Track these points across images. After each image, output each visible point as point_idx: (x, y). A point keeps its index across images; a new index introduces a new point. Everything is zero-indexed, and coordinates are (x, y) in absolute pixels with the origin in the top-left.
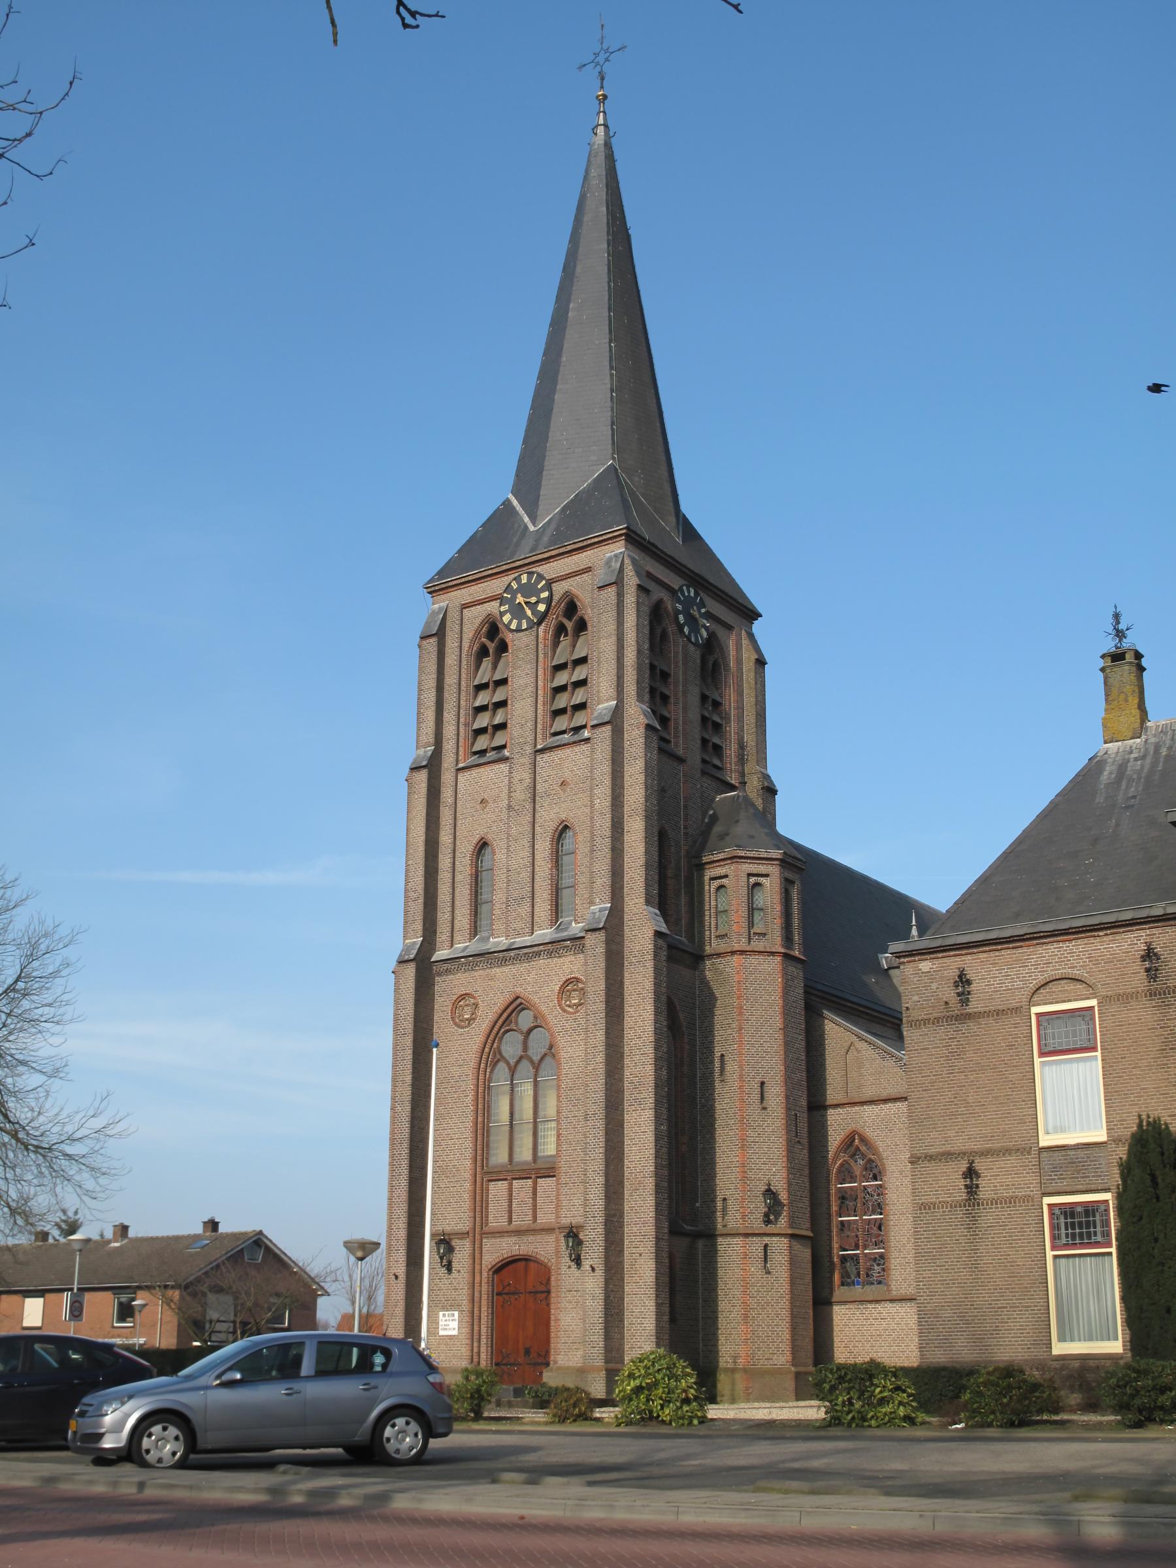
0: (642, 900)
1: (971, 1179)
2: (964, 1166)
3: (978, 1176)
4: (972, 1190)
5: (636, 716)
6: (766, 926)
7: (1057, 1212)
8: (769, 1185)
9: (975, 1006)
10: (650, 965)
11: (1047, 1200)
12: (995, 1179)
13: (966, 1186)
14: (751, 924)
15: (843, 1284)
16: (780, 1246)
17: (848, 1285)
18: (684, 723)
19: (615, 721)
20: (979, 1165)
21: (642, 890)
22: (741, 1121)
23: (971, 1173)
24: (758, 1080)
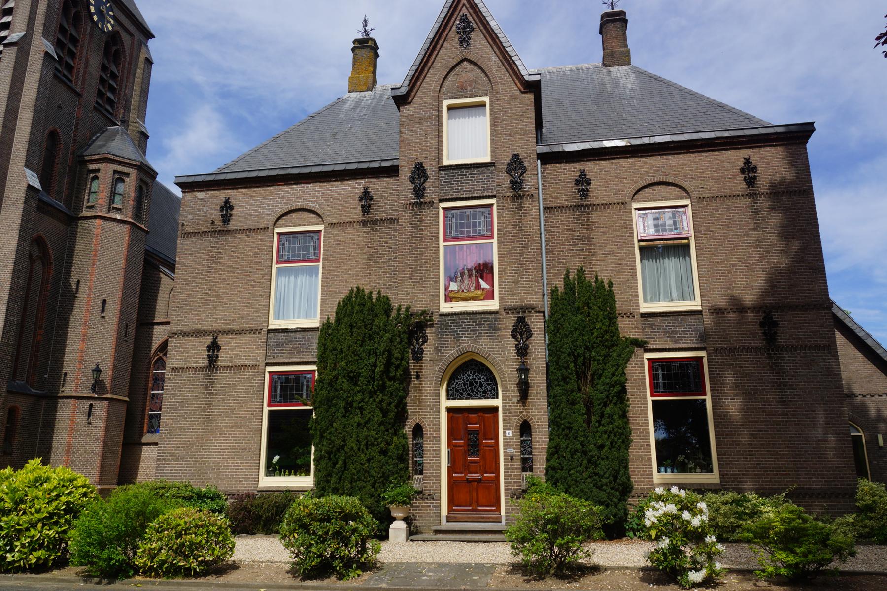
0: (23, 164)
1: (214, 351)
2: (209, 340)
3: (219, 350)
4: (213, 359)
5: (41, 45)
6: (123, 203)
7: (276, 377)
8: (97, 365)
9: (234, 224)
10: (21, 206)
11: (269, 369)
12: (232, 351)
13: (209, 356)
14: (112, 201)
15: (148, 432)
16: (101, 408)
17: (152, 433)
18: (85, 73)
19: (23, 46)
20: (222, 340)
21: (24, 157)
22: (85, 324)
23: (214, 347)
24: (102, 298)
